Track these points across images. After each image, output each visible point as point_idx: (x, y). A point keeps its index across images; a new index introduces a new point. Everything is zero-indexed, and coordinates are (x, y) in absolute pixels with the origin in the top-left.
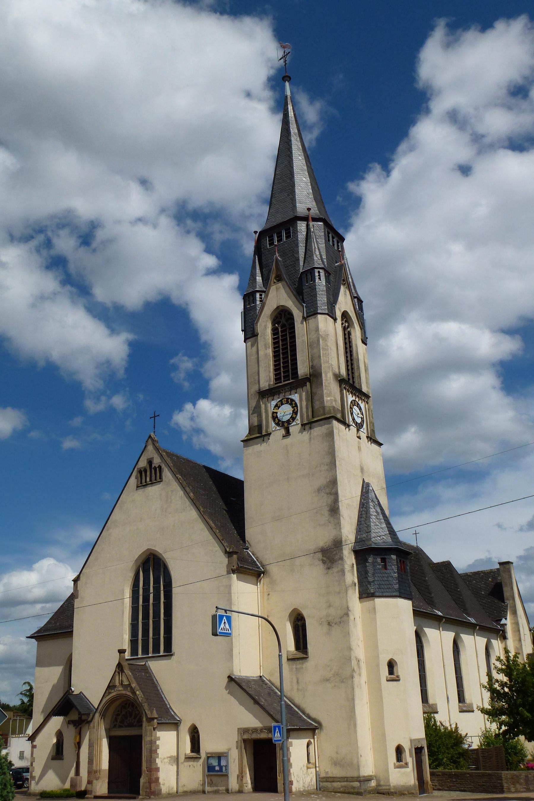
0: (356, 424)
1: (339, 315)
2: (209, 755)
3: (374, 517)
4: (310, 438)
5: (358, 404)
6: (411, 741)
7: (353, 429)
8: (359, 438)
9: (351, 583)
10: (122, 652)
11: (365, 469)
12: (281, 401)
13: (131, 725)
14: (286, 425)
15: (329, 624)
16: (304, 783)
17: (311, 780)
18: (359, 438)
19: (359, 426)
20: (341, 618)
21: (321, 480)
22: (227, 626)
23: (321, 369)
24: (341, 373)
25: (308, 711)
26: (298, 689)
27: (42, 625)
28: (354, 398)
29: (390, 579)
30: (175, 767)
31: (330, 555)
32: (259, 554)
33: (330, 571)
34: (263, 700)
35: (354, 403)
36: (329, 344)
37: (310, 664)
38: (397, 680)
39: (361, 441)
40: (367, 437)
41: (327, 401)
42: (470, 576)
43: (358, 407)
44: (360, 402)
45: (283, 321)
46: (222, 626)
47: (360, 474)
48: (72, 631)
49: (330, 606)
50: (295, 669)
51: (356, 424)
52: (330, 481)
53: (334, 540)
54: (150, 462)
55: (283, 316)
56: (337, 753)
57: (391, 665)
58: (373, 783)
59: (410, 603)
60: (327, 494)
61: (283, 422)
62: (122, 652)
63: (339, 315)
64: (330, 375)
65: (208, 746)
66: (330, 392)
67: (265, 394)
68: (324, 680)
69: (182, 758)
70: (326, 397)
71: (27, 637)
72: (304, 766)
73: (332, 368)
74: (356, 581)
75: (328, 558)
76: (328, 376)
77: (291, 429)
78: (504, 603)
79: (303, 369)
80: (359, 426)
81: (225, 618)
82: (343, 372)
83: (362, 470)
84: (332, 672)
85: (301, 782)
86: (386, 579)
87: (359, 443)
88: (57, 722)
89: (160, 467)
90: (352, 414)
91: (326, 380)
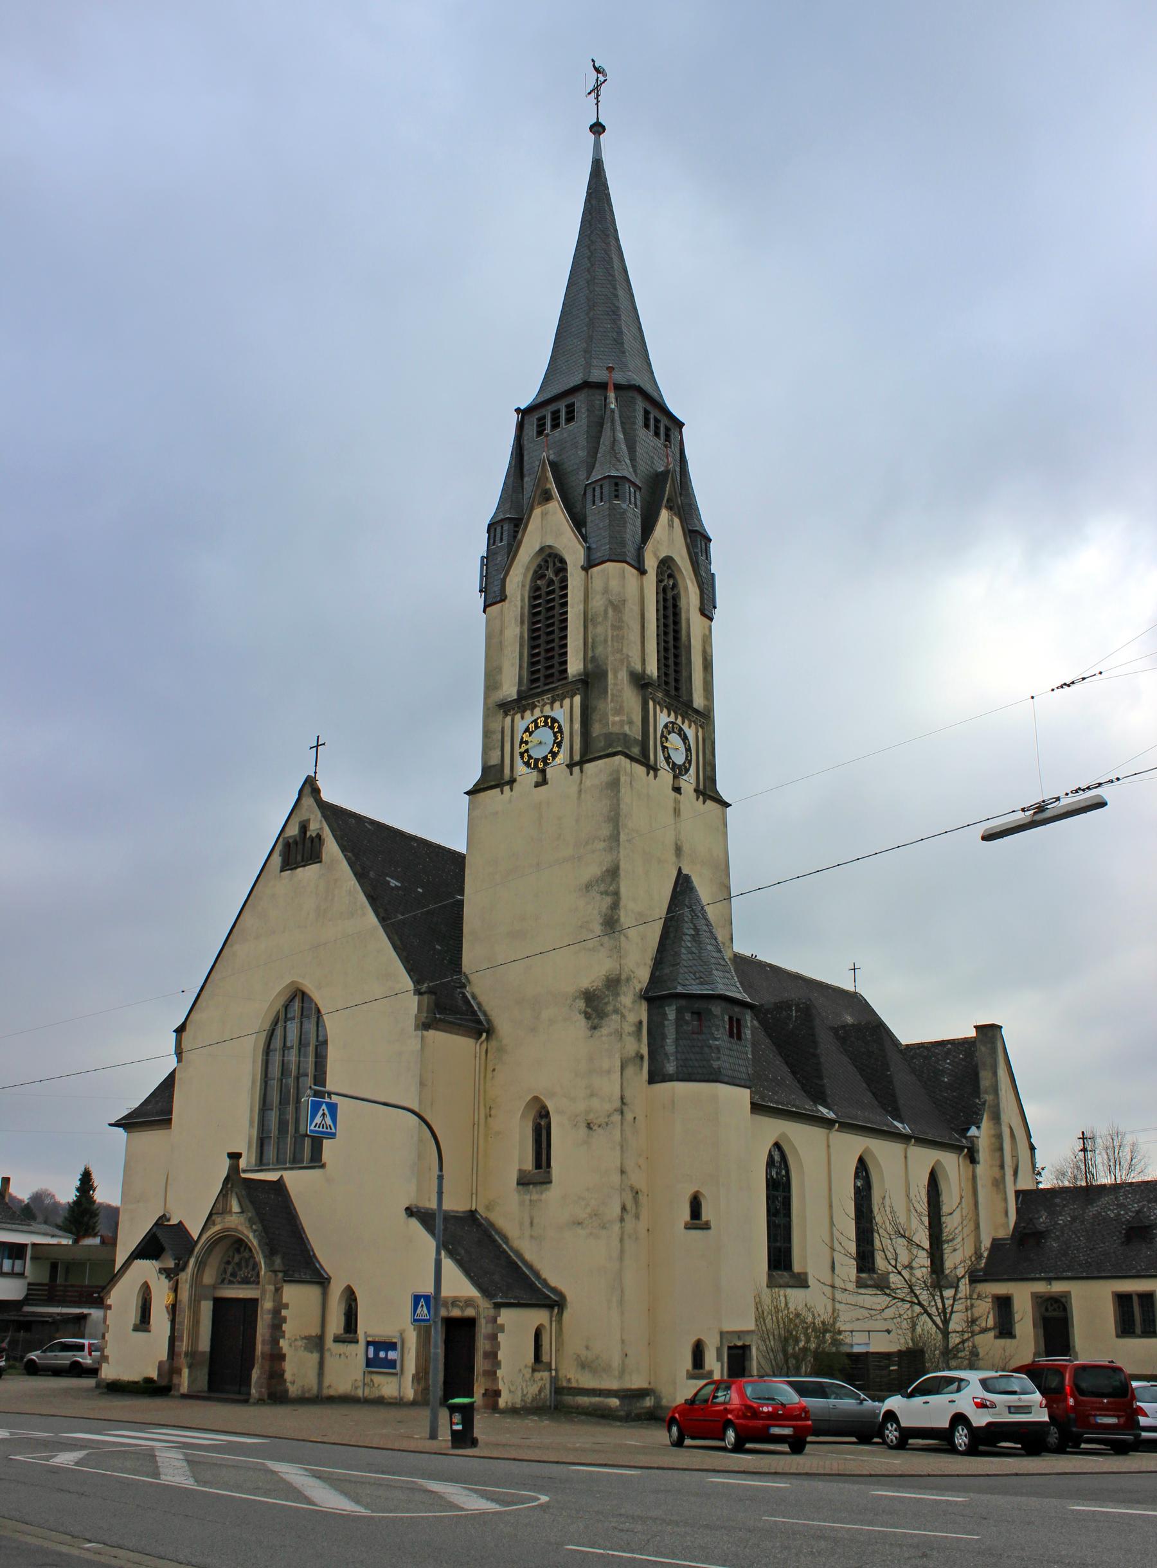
0: (674, 766)
1: (651, 564)
2: (369, 1339)
4: (580, 791)
5: (681, 729)
6: (722, 1334)
7: (666, 776)
8: (677, 790)
9: (634, 1055)
10: (235, 1156)
11: (686, 848)
12: (535, 721)
13: (246, 1281)
14: (540, 767)
15: (589, 1126)
16: (524, 1395)
17: (540, 1392)
18: (677, 790)
19: (679, 771)
20: (609, 1116)
21: (593, 869)
22: (328, 1120)
23: (606, 664)
24: (648, 672)
26: (532, 1237)
27: (137, 1106)
28: (672, 719)
29: (706, 1050)
30: (315, 1356)
31: (594, 1006)
32: (481, 998)
33: (597, 1033)
34: (463, 1252)
35: (670, 728)
36: (625, 618)
37: (553, 1194)
38: (706, 1226)
39: (681, 798)
40: (696, 791)
41: (614, 723)
42: (926, 1048)
43: (680, 735)
44: (685, 727)
45: (550, 574)
46: (318, 1119)
47: (673, 859)
48: (171, 1119)
49: (592, 1095)
50: (527, 1202)
51: (674, 766)
52: (608, 871)
53: (607, 977)
54: (304, 827)
55: (551, 565)
56: (587, 1348)
58: (648, 1402)
59: (748, 1091)
60: (602, 893)
61: (537, 761)
62: (235, 1156)
63: (651, 564)
64: (623, 675)
65: (366, 1327)
67: (506, 708)
68: (574, 1223)
70: (613, 715)
71: (111, 1125)
72: (526, 1366)
73: (629, 663)
74: (645, 1051)
75: (595, 1009)
76: (620, 677)
77: (549, 771)
78: (979, 1098)
79: (574, 666)
80: (679, 771)
81: (324, 1107)
82: (652, 669)
83: (678, 851)
84: (589, 1210)
85: (519, 1393)
86: (697, 1049)
87: (677, 802)
88: (146, 1269)
89: (319, 836)
90: (688, 750)
91: (615, 684)
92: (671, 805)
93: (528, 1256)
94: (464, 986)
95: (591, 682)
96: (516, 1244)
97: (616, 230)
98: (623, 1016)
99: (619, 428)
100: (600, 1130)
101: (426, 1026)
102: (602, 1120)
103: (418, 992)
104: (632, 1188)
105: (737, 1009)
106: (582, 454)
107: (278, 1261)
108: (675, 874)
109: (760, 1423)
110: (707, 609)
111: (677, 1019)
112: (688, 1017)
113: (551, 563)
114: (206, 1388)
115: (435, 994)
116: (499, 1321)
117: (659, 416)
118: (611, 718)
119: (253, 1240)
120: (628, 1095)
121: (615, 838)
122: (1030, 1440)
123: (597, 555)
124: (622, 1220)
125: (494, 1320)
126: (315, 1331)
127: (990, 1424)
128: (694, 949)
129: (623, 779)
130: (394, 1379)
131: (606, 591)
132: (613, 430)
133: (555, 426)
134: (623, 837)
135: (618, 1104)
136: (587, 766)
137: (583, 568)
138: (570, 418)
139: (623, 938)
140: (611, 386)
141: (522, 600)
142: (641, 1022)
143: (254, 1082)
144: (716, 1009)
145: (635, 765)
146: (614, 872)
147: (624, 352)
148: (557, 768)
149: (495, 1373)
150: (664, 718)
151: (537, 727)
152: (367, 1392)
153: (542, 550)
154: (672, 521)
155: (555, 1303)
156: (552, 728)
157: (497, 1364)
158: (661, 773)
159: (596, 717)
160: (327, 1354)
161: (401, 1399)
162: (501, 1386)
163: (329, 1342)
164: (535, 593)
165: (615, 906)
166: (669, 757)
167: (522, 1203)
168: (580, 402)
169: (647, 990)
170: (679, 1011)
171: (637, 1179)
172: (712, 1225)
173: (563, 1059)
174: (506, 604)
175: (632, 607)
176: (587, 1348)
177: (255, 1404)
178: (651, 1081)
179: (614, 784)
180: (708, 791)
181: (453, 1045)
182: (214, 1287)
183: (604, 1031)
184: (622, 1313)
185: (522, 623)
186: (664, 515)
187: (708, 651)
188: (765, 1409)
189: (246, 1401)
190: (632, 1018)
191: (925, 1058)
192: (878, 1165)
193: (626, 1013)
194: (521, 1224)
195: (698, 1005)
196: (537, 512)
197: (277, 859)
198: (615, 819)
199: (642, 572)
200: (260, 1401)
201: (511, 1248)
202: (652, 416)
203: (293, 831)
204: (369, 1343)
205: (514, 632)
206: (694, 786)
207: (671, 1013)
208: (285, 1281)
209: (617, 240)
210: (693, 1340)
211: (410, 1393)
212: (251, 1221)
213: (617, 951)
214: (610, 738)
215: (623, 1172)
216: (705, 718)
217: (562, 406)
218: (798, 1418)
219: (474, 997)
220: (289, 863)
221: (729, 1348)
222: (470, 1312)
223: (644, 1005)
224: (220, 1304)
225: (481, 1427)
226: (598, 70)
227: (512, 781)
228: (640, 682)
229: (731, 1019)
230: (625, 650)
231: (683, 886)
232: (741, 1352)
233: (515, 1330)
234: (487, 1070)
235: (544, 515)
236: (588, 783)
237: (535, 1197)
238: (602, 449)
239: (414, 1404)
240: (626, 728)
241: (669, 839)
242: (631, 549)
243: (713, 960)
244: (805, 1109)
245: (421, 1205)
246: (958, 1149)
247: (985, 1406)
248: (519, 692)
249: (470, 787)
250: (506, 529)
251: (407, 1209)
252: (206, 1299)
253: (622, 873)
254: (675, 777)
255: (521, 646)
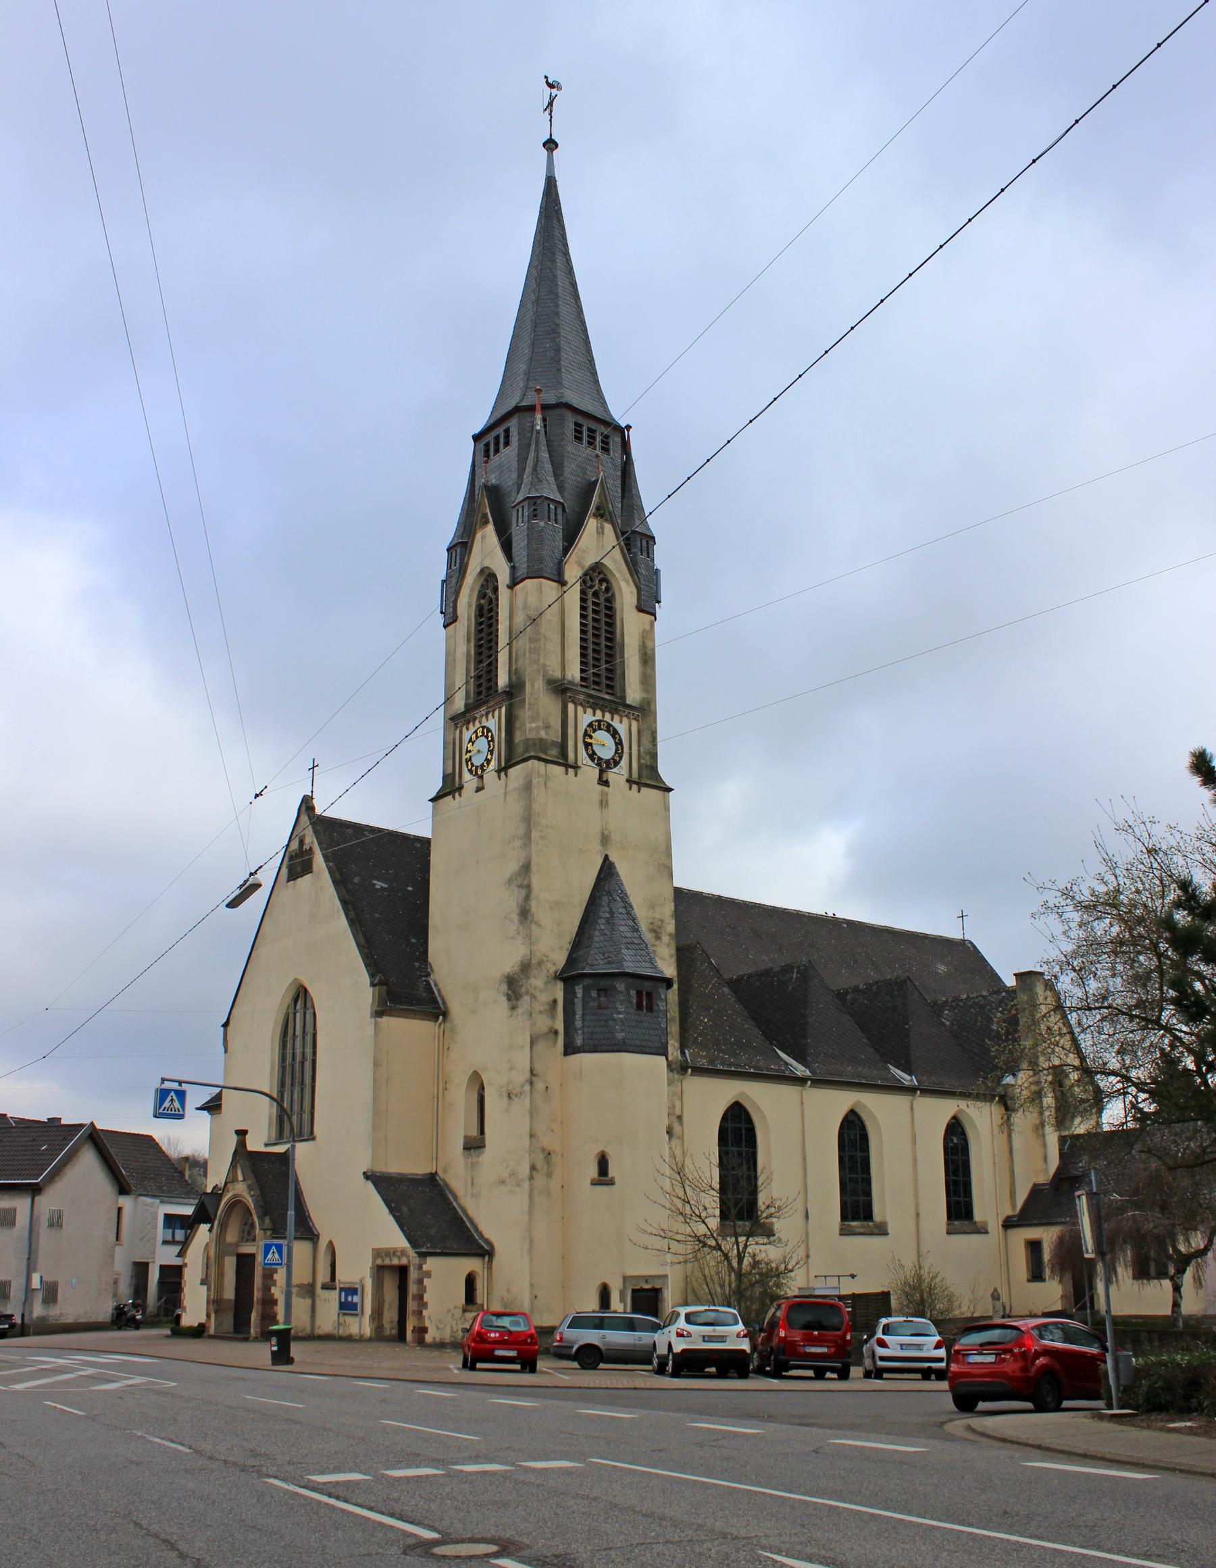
1: (573, 573)
3: (603, 921)
5: (609, 725)
6: (625, 1278)
7: (590, 772)
8: (604, 782)
12: (476, 732)
19: (603, 766)
21: (513, 866)
25: (482, 1227)
26: (472, 1195)
29: (611, 1023)
32: (441, 986)
33: (515, 1013)
35: (593, 727)
36: (542, 630)
38: (611, 1183)
39: (609, 790)
43: (608, 731)
44: (615, 723)
47: (599, 847)
54: (302, 842)
56: (508, 1291)
57: (603, 1164)
62: (242, 1133)
63: (573, 573)
64: (540, 684)
65: (343, 1276)
66: (538, 713)
69: (319, 1285)
73: (546, 672)
74: (560, 1026)
79: (502, 680)
81: (172, 1093)
82: (574, 672)
83: (605, 839)
92: (596, 797)
93: (471, 1212)
94: (428, 975)
95: (515, 690)
96: (463, 1201)
97: (566, 245)
98: (533, 997)
99: (543, 447)
100: (516, 1100)
101: (379, 1014)
102: (518, 1090)
103: (373, 985)
104: (543, 1149)
105: (647, 984)
106: (514, 476)
107: (267, 1220)
108: (599, 862)
109: (487, 1346)
110: (648, 603)
111: (583, 996)
112: (594, 994)
113: (488, 578)
114: (232, 1329)
115: (386, 984)
116: (425, 1267)
117: (593, 425)
118: (528, 725)
119: (252, 1206)
120: (538, 1068)
121: (527, 836)
122: (730, 1364)
123: (521, 572)
124: (531, 1178)
125: (420, 1267)
126: (307, 1280)
127: (684, 1351)
128: (607, 932)
129: (535, 781)
130: (357, 1319)
131: (525, 607)
132: (537, 451)
133: (497, 451)
134: (534, 834)
135: (528, 1075)
136: (511, 771)
137: (509, 587)
138: (507, 444)
139: (534, 927)
140: (539, 408)
141: (469, 620)
142: (555, 1001)
143: (272, 1068)
144: (620, 986)
145: (550, 766)
146: (526, 868)
147: (559, 370)
148: (490, 775)
149: (421, 1312)
150: (587, 717)
151: (477, 737)
152: (342, 1332)
153: (482, 571)
154: (602, 528)
155: (485, 1252)
156: (487, 737)
157: (425, 1305)
158: (584, 770)
159: (517, 725)
160: (317, 1300)
161: (362, 1336)
162: (427, 1323)
163: (319, 1291)
164: (480, 611)
165: (527, 898)
166: (594, 753)
167: (466, 1166)
168: (513, 424)
169: (563, 971)
170: (586, 990)
171: (548, 1141)
172: (616, 1181)
173: (491, 1034)
174: (457, 623)
175: (552, 616)
176: (508, 1291)
177: (253, 1341)
178: (566, 1054)
179: (528, 787)
180: (648, 777)
181: (409, 1030)
182: (237, 1245)
183: (520, 1011)
184: (531, 1261)
185: (469, 640)
186: (591, 524)
187: (649, 644)
188: (493, 1335)
189: (246, 1340)
190: (544, 998)
191: (982, 1007)
192: (873, 1117)
193: (537, 994)
194: (466, 1184)
195: (603, 983)
196: (479, 536)
197: (285, 871)
198: (528, 819)
199: (562, 583)
200: (256, 1339)
201: (459, 1205)
202: (585, 429)
203: (295, 845)
204: (341, 1289)
205: (463, 649)
206: (626, 776)
207: (579, 991)
208: (296, 1238)
209: (566, 254)
210: (598, 1282)
211: (367, 1331)
212: (250, 1188)
213: (529, 939)
214: (528, 744)
215: (531, 1136)
216: (645, 712)
217: (500, 430)
218: (524, 1342)
219: (436, 985)
220: (293, 875)
221: (634, 1291)
222: (404, 1261)
223: (560, 985)
224: (240, 1257)
225: (296, 1349)
226: (551, 86)
227: (461, 788)
228: (560, 689)
229: (639, 994)
230: (541, 661)
231: (607, 870)
232: (652, 1294)
233: (443, 1279)
234: (443, 1049)
235: (483, 537)
236: (511, 786)
237: (474, 1160)
238: (528, 470)
239: (370, 1340)
240: (543, 734)
241: (595, 829)
242: (550, 566)
243: (625, 940)
244: (768, 1069)
245: (377, 1169)
246: (987, 1097)
247: (682, 1336)
248: (466, 705)
249: (433, 795)
250: (460, 549)
251: (364, 1173)
252: (229, 1254)
253: (534, 868)
254: (602, 772)
255: (468, 662)
